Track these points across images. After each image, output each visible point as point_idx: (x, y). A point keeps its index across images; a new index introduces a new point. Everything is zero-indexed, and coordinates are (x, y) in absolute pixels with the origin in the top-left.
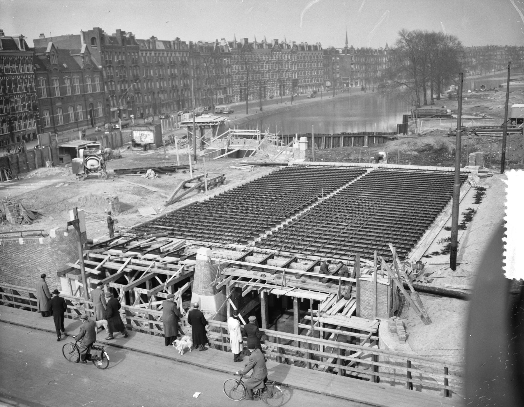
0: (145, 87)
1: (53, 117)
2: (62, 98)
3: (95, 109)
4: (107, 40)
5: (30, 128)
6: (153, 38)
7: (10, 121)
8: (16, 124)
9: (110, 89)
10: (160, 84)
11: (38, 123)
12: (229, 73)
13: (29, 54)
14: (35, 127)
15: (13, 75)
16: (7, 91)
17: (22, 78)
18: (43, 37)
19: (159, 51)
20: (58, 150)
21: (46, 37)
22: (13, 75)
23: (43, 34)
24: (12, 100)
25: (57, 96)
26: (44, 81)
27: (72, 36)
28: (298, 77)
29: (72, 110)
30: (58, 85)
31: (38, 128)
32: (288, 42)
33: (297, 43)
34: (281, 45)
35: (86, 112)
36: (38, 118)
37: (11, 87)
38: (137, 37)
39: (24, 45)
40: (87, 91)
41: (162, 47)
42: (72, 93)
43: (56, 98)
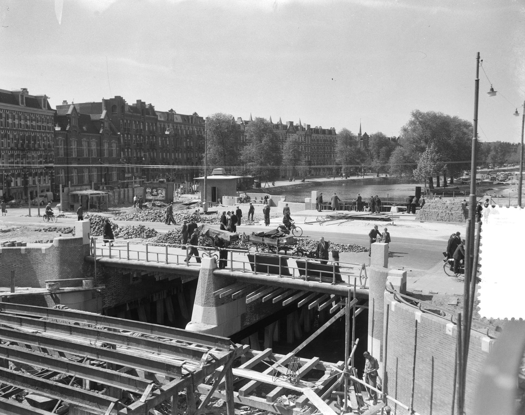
0: (160, 157)
1: (68, 176)
2: (79, 159)
3: (110, 173)
4: (126, 109)
5: (44, 185)
6: (172, 110)
7: (25, 175)
8: (30, 179)
9: (126, 189)
10: (175, 155)
11: (52, 181)
12: (243, 140)
13: (51, 114)
14: (49, 184)
15: (33, 132)
16: (25, 146)
17: (41, 136)
18: (65, 104)
19: (177, 123)
20: (70, 197)
21: (68, 104)
22: (33, 132)
23: (66, 101)
24: (29, 155)
25: (74, 156)
26: (63, 141)
27: (94, 104)
28: (311, 159)
29: (87, 172)
30: (75, 147)
31: (52, 185)
32: (302, 125)
33: (312, 127)
34: (297, 127)
35: (101, 175)
36: (53, 176)
37: (29, 142)
38: (156, 109)
39: (46, 105)
40: (104, 155)
41: (180, 120)
42: (89, 155)
43: (73, 158)
